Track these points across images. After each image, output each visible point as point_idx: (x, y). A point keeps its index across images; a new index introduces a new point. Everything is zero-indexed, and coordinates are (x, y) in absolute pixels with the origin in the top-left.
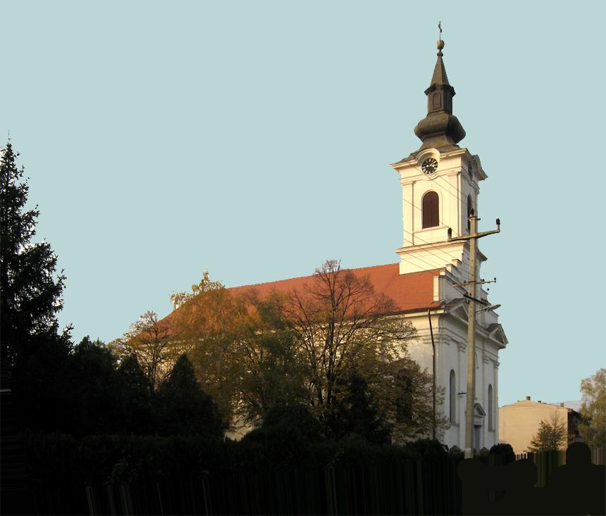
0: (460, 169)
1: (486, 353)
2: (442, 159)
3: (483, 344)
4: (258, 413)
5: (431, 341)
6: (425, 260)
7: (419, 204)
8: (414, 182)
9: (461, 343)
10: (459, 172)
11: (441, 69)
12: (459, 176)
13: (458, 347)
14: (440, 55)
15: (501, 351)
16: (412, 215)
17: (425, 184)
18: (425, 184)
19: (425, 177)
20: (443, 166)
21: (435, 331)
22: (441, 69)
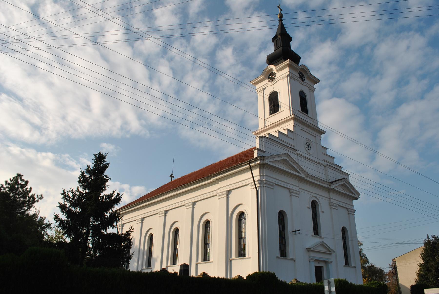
0: (288, 74)
1: (333, 201)
2: (278, 71)
3: (330, 195)
4: (100, 220)
5: (254, 187)
6: (201, 34)
7: (267, 97)
8: (264, 89)
9: (292, 189)
10: (288, 76)
11: (282, 28)
12: (288, 78)
13: (290, 193)
14: (281, 21)
15: (354, 202)
16: (263, 104)
17: (270, 87)
18: (270, 87)
19: (270, 84)
20: (278, 75)
21: (256, 179)
22: (282, 28)
